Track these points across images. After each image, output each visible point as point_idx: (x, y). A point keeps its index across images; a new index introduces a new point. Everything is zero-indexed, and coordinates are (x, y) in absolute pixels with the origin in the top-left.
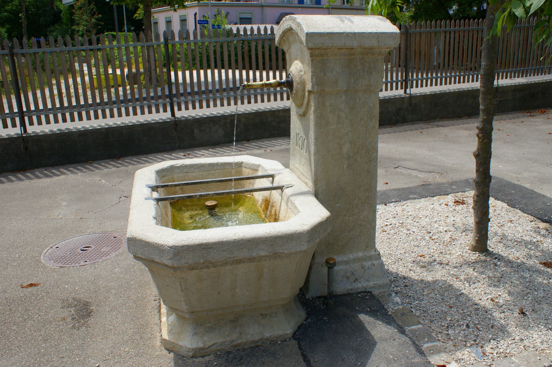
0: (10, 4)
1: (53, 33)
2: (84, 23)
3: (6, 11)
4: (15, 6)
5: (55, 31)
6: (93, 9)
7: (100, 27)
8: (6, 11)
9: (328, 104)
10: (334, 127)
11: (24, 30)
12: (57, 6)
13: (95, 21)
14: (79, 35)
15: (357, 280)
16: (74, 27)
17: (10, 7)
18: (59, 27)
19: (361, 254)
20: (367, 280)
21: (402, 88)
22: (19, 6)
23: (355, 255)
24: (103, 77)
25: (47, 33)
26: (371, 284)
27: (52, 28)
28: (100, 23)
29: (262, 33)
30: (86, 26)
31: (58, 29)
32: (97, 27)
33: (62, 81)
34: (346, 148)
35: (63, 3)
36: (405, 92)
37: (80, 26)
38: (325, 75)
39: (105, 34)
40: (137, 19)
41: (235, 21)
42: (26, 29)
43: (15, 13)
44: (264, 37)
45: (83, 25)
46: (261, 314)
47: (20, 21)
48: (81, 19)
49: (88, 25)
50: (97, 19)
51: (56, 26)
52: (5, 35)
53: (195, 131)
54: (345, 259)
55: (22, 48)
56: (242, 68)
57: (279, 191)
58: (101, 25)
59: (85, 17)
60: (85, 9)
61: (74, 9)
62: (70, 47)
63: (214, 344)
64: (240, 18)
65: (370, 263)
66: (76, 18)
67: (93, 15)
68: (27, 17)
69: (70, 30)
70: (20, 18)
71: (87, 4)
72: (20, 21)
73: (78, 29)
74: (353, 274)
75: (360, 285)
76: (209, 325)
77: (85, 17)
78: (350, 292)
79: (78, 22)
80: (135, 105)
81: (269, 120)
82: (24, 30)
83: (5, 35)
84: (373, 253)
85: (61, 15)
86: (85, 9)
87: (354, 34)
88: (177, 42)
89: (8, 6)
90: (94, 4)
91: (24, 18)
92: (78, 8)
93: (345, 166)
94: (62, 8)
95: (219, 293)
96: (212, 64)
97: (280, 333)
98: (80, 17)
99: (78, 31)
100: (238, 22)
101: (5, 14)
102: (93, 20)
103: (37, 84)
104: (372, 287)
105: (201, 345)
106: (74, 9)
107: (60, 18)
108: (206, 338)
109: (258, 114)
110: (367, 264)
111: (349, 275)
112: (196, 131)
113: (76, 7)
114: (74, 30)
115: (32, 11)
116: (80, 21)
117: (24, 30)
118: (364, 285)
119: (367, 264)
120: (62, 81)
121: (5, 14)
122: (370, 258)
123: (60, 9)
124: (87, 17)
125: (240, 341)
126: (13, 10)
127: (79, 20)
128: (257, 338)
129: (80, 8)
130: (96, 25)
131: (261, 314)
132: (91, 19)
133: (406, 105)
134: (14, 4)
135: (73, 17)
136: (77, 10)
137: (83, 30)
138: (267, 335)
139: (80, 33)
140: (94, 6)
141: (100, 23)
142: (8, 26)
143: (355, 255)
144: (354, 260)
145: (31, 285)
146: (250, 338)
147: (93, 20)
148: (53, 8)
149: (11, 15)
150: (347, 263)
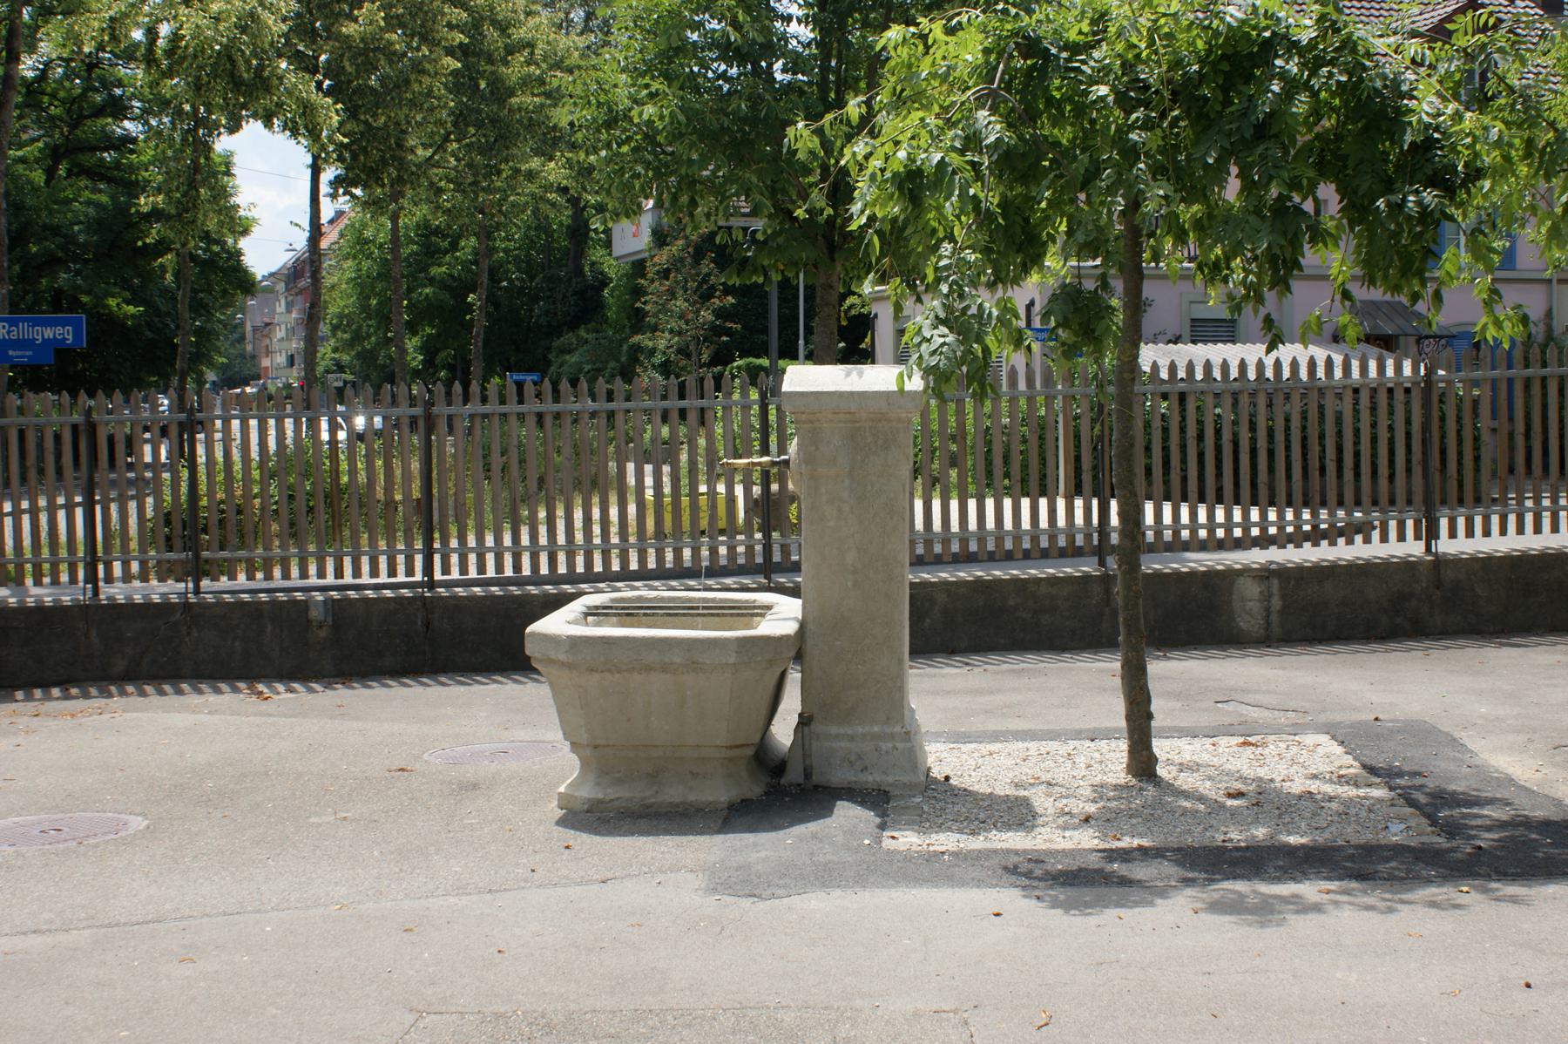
0: (448, 258)
1: (568, 357)
2: (673, 324)
3: (432, 281)
4: (462, 263)
5: (576, 349)
6: (708, 275)
7: (725, 338)
8: (432, 281)
9: (823, 490)
10: (832, 523)
11: (476, 346)
12: (593, 264)
13: (711, 318)
14: (653, 365)
15: (866, 768)
16: (637, 339)
17: (444, 269)
18: (590, 336)
19: (876, 729)
20: (884, 773)
21: (1417, 537)
22: (472, 263)
23: (867, 729)
24: (685, 500)
25: (550, 356)
26: (890, 779)
27: (568, 338)
28: (728, 325)
29: (1269, 374)
30: (680, 333)
31: (586, 342)
32: (715, 339)
33: (560, 512)
34: (850, 557)
35: (615, 254)
36: (1428, 549)
37: (658, 333)
38: (817, 449)
39: (735, 364)
40: (853, 312)
41: (1172, 331)
42: (480, 344)
43: (458, 288)
44: (1218, 387)
45: (671, 331)
46: (691, 773)
47: (468, 317)
48: (664, 309)
49: (687, 331)
50: (720, 313)
51: (582, 333)
52: (414, 359)
54: (849, 732)
55: (449, 404)
56: (1249, 502)
57: (455, 420)
58: (729, 332)
59: (680, 304)
60: (680, 277)
61: (643, 276)
62: (512, 407)
63: (618, 799)
64: (1193, 320)
65: (890, 745)
66: (648, 308)
67: (706, 296)
68: (492, 300)
69: (625, 347)
70: (469, 308)
71: (689, 260)
72: (468, 317)
73: (650, 344)
74: (860, 758)
75: (870, 778)
76: (617, 775)
77: (680, 304)
78: (853, 786)
79: (653, 321)
80: (680, 545)
81: (1011, 603)
82: (475, 348)
83: (414, 359)
84: (897, 729)
85: (606, 292)
86: (680, 277)
87: (852, 393)
88: (1022, 393)
89: (440, 265)
90: (713, 261)
91: (480, 308)
92: (658, 273)
93: (850, 584)
94: (611, 268)
95: (629, 720)
96: (1263, 492)
97: (711, 799)
98: (663, 305)
99: (652, 352)
100: (1186, 334)
101: (427, 291)
102: (706, 315)
103: (489, 517)
104: (891, 785)
105: (600, 796)
106: (643, 276)
107: (600, 305)
108: (609, 791)
110: (886, 745)
111: (853, 758)
113: (651, 271)
114: (637, 348)
115: (511, 281)
116: (661, 316)
117: (475, 348)
118: (878, 779)
119: (886, 745)
120: (560, 512)
121: (427, 291)
122: (892, 736)
123: (602, 273)
124: (686, 304)
125: (653, 800)
126: (453, 276)
127: (655, 315)
128: (677, 800)
129: (665, 274)
130: (716, 331)
131: (691, 773)
132: (698, 311)
133: (1424, 585)
134: (457, 258)
135: (638, 305)
136: (653, 281)
137: (668, 348)
138: (692, 798)
139: (658, 359)
140: (712, 265)
141: (728, 325)
142: (428, 330)
143: (867, 729)
144: (864, 735)
145: (402, 770)
146: (668, 799)
147: (706, 315)
148: (579, 271)
149: (445, 296)
150: (852, 738)
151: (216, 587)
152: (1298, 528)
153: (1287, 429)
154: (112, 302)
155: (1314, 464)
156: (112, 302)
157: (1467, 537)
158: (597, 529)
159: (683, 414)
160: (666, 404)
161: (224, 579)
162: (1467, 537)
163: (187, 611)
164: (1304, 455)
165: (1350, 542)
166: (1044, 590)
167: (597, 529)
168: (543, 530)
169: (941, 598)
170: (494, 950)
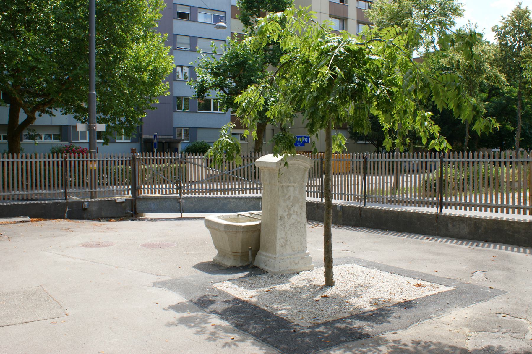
53: (449, 225)
81: (505, 228)
109: (496, 222)
112: (450, 225)
151: (446, 211)
152: (188, 191)
153: (318, 165)
154: (508, 127)
155: (250, 175)
156: (508, 127)
157: (512, 213)
158: (522, 201)
159: (511, 163)
160: (495, 160)
161: (193, 194)
162: (512, 213)
163: (437, 217)
164: (248, 172)
165: (451, 208)
166: (516, 225)
167: (522, 201)
168: (409, 195)
169: (484, 224)
170: (453, 318)
